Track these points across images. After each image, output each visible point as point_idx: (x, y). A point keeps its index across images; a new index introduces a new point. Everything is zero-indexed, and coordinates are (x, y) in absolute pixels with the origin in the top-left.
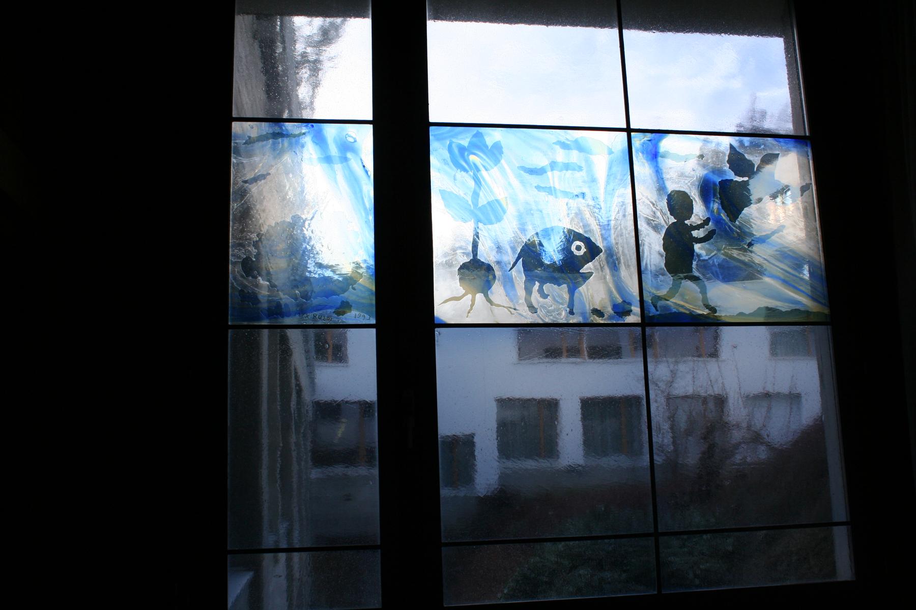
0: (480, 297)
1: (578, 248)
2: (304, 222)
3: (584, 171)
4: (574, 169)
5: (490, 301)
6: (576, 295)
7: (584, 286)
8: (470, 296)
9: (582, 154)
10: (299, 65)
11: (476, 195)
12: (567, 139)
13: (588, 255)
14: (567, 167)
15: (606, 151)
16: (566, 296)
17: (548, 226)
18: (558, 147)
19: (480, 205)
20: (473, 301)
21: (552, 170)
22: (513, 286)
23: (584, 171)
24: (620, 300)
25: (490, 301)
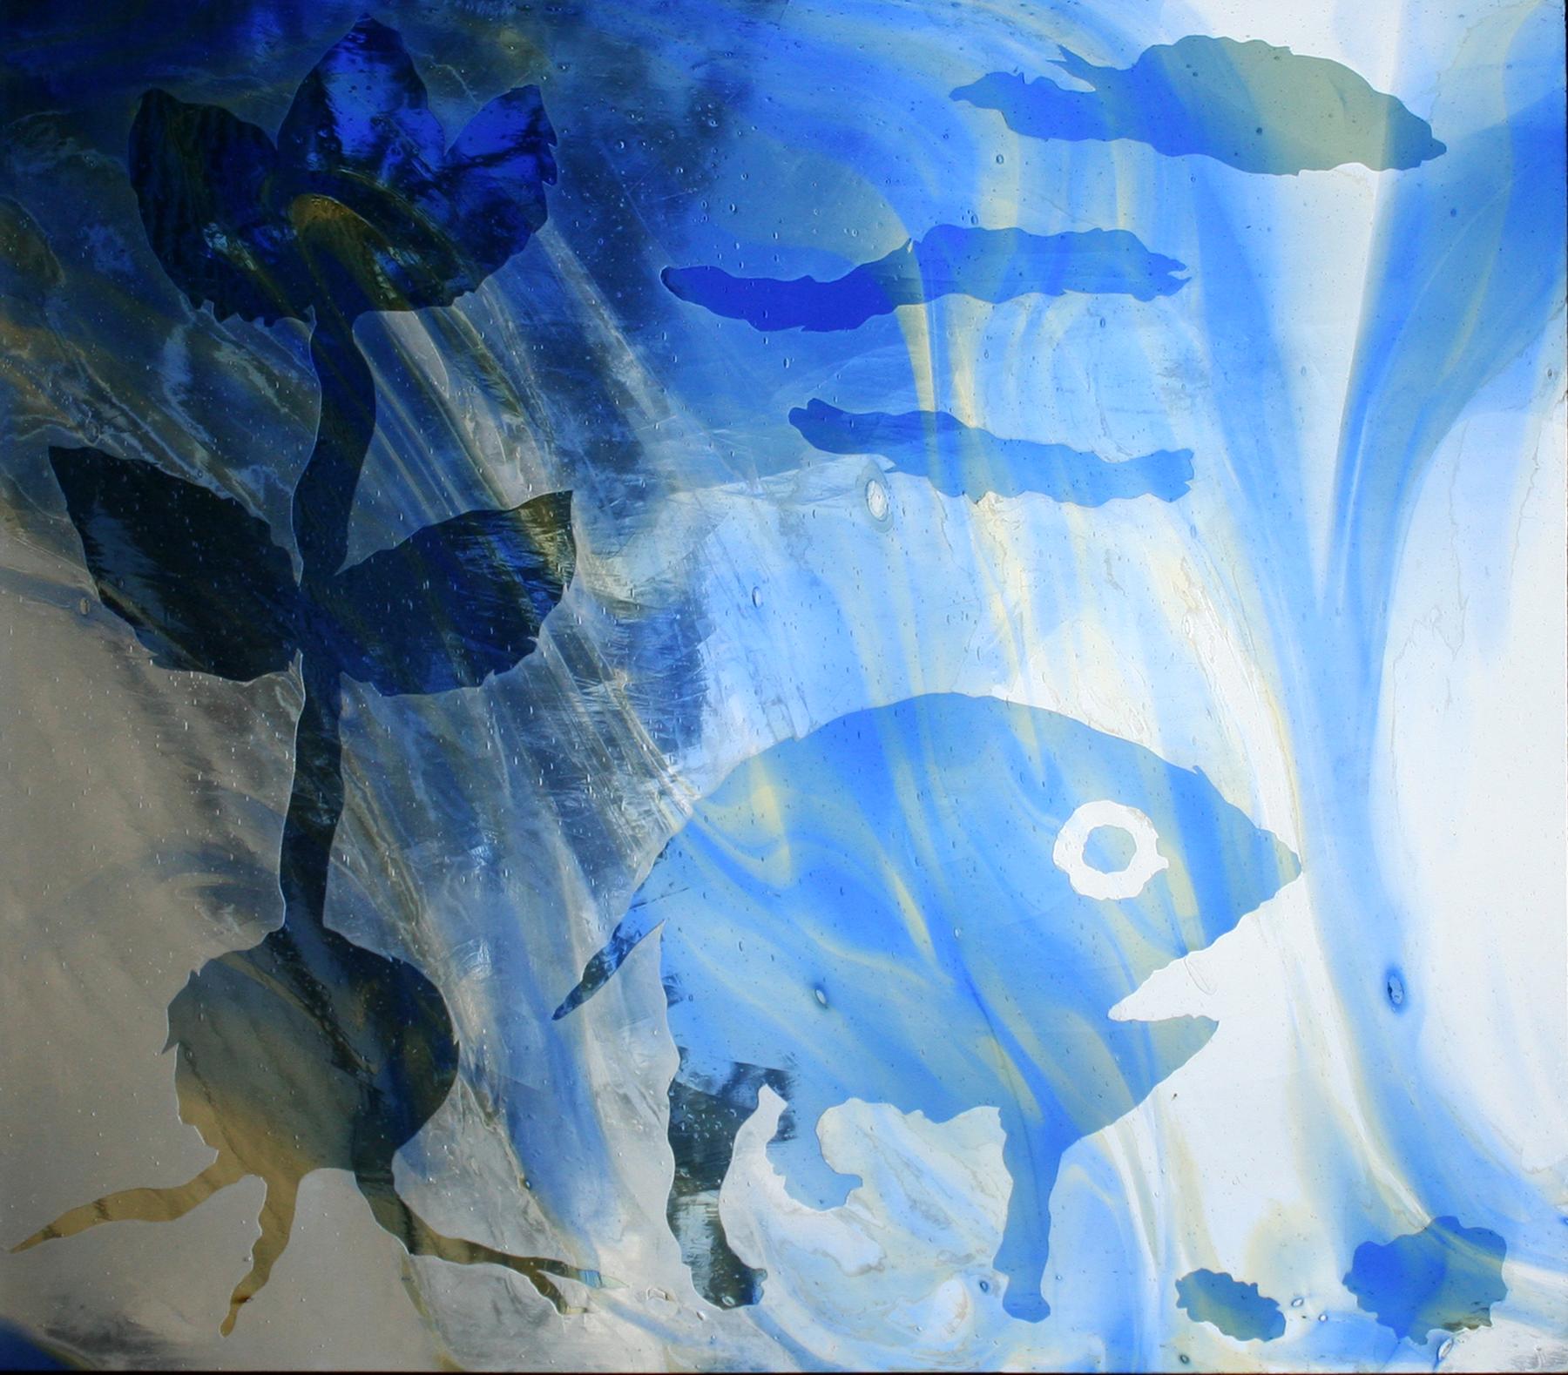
0: (328, 1193)
1: (1106, 852)
2: (577, 789)
3: (1192, 293)
4: (1111, 283)
5: (411, 1232)
6: (1072, 1172)
7: (1137, 1119)
8: (253, 1190)
9: (1185, 164)
10: (602, 812)
11: (328, 485)
12: (1074, 64)
13: (1186, 903)
14: (1056, 262)
15: (1380, 133)
16: (995, 1187)
17: (878, 696)
18: (990, 126)
19: (356, 554)
20: (279, 1217)
21: (938, 287)
22: (535, 336)
23: (1192, 293)
24: (1408, 1213)
25: (411, 1232)
